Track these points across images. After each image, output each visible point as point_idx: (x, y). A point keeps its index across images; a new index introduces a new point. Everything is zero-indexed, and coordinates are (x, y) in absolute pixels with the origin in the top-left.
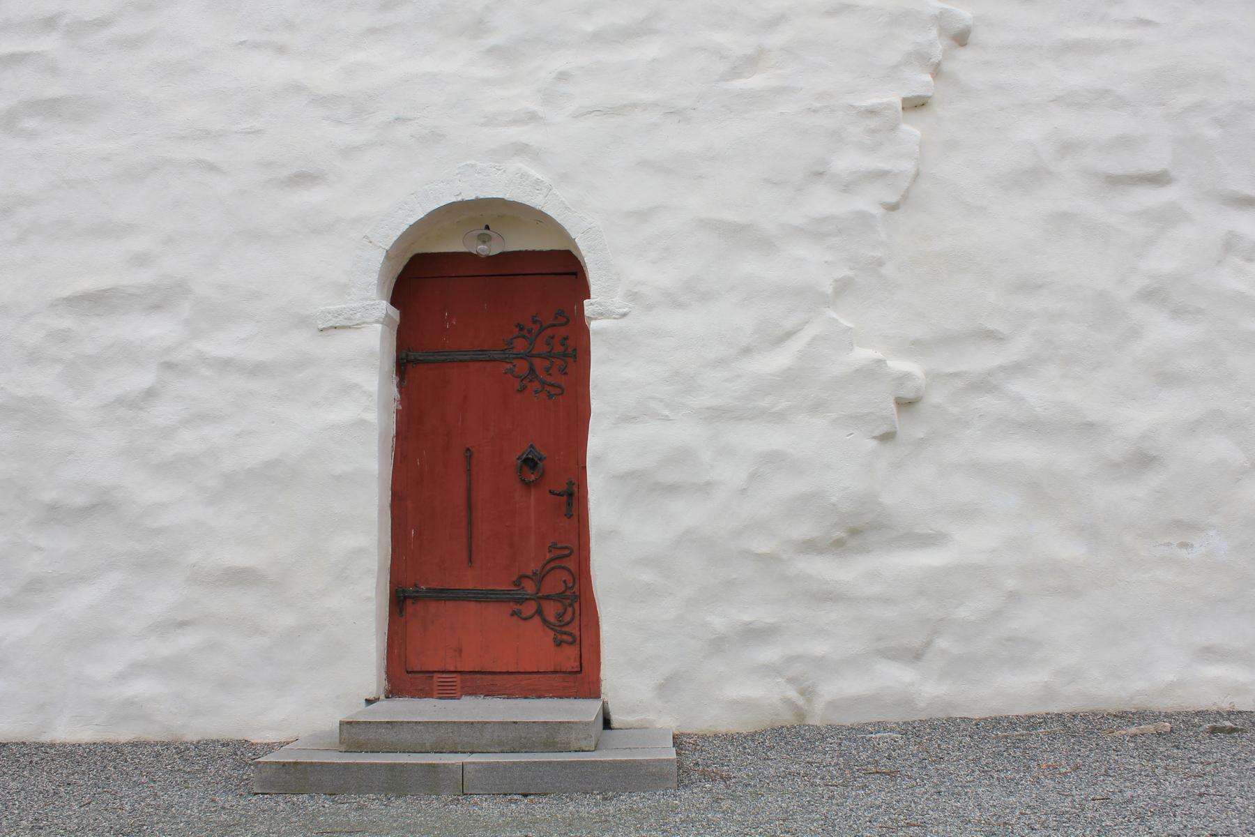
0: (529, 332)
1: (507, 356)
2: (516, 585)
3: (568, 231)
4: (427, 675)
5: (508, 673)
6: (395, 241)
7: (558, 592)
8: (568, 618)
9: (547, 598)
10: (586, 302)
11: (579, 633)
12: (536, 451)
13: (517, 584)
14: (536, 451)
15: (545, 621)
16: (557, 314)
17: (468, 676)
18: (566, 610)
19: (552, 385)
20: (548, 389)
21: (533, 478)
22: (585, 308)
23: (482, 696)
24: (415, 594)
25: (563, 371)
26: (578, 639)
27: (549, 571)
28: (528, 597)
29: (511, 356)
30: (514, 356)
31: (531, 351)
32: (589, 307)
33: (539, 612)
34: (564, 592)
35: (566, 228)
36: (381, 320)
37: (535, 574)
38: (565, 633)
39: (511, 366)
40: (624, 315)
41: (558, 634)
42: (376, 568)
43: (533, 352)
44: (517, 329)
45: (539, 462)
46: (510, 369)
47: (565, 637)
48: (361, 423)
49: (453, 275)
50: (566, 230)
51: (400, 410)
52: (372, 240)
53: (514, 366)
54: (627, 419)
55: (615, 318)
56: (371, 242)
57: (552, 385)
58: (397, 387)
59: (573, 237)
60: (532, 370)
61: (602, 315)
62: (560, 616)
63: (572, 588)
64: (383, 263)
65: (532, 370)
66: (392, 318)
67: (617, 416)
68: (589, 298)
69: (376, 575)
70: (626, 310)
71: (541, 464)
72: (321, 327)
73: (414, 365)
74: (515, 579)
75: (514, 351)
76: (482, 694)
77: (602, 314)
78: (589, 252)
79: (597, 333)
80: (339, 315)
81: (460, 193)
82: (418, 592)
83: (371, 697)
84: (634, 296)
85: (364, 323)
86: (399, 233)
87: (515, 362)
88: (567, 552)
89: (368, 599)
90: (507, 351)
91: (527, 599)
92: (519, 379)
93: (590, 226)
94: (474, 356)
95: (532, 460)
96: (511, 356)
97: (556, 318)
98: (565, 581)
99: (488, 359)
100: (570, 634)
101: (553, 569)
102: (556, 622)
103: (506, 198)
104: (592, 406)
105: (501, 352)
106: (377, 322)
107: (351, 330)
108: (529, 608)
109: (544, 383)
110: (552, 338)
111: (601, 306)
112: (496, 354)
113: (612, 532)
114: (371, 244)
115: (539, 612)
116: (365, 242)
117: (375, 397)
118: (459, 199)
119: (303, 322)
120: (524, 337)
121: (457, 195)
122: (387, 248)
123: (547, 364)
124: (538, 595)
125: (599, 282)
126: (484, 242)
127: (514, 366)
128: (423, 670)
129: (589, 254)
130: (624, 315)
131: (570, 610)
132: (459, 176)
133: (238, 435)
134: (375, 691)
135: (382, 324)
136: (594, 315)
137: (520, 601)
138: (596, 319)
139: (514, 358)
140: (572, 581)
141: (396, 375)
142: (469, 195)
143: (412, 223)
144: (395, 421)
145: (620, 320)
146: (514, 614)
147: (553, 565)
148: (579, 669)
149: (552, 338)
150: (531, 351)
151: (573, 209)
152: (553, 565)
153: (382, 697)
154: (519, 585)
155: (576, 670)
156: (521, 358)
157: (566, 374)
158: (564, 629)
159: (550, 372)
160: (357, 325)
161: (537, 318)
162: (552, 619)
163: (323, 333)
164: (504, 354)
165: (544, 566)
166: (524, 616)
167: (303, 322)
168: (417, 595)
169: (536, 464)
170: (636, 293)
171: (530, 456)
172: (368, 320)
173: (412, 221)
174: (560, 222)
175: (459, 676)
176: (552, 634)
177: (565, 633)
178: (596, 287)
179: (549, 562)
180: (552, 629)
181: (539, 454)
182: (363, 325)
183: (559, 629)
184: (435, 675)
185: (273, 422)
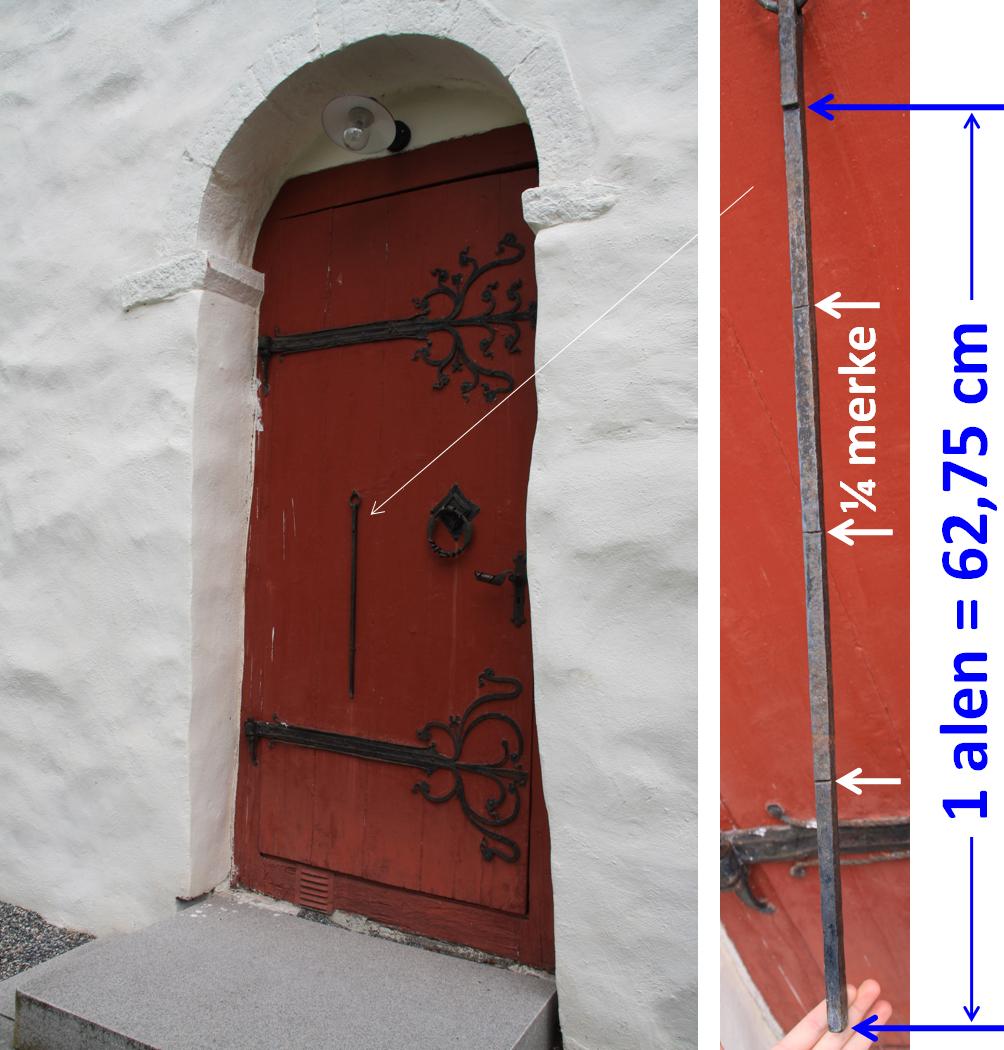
0: (456, 281)
1: (418, 328)
2: (421, 740)
3: (496, 64)
4: (289, 865)
5: (404, 889)
6: (224, 151)
7: (492, 764)
8: (508, 810)
9: (473, 770)
10: (527, 194)
11: (526, 845)
12: (463, 498)
13: (425, 736)
14: (463, 498)
15: (468, 812)
16: (501, 243)
17: (345, 881)
18: (504, 798)
19: (492, 375)
20: (484, 380)
21: (457, 547)
22: (525, 206)
23: (364, 919)
24: (271, 733)
25: (511, 348)
26: (524, 855)
27: (479, 721)
28: (442, 764)
29: (425, 328)
30: (430, 327)
31: (457, 316)
32: (533, 204)
33: (459, 794)
34: (501, 765)
35: (492, 60)
36: (201, 282)
37: (454, 724)
38: (501, 840)
39: (426, 346)
40: (604, 209)
41: (490, 840)
42: (190, 694)
43: (461, 317)
44: (437, 279)
45: (465, 519)
46: (424, 349)
47: (500, 847)
48: (169, 455)
49: (340, 204)
50: (492, 63)
51: (261, 433)
52: (192, 155)
53: (430, 345)
54: (612, 430)
55: (584, 219)
56: (191, 160)
57: (492, 375)
58: (259, 396)
59: (505, 75)
60: (458, 349)
61: (559, 216)
62: (494, 807)
63: (515, 759)
64: (209, 192)
65: (458, 349)
66: (239, 282)
67: (589, 425)
68: (536, 184)
69: (190, 705)
70: (609, 198)
71: (468, 524)
72: (125, 305)
73: (282, 358)
74: (421, 728)
75: (430, 319)
76: (365, 916)
77: (558, 215)
78: (536, 96)
79: (548, 254)
80: (147, 282)
81: (318, 46)
82: (276, 730)
83: (186, 895)
84: (625, 168)
85: (178, 290)
86: (229, 136)
87: (431, 338)
88: (511, 690)
89: (178, 743)
90: (418, 321)
91: (440, 767)
92: (437, 368)
93: (536, 44)
94: (367, 335)
95: (452, 514)
96: (425, 328)
97: (502, 251)
98: (505, 744)
99: (388, 337)
100: (512, 844)
101: (485, 717)
102: (487, 817)
103: (388, 33)
104: (541, 407)
105: (410, 323)
106: (196, 286)
107: (164, 305)
108: (444, 785)
109: (478, 372)
110: (494, 287)
111: (556, 196)
112: (399, 327)
113: (572, 670)
114: (191, 163)
115: (459, 794)
116: (185, 162)
117: (190, 411)
118: (317, 55)
119: (105, 300)
120: (447, 292)
121: (313, 50)
122: (213, 164)
123: (484, 335)
124: (457, 762)
125: (555, 152)
126: (359, 125)
127: (430, 345)
128: (281, 855)
129: (536, 100)
130: (604, 209)
131: (511, 797)
132: (316, 17)
133: (31, 477)
134: (188, 888)
135: (205, 288)
136: (541, 218)
137: (431, 769)
138: (545, 226)
139: (429, 332)
140: (517, 745)
141: (258, 377)
142: (331, 44)
143: (247, 115)
144: (254, 450)
145: (596, 221)
146: (418, 789)
147: (486, 710)
148: (523, 912)
149: (494, 287)
150: (457, 316)
151: (505, 19)
152: (486, 710)
153: (224, 888)
154: (428, 740)
155: (516, 911)
156: (443, 330)
157: (517, 352)
158: (501, 832)
159: (491, 350)
160: (170, 295)
161: (469, 256)
162: (481, 811)
163: (130, 314)
164: (413, 325)
165: (469, 713)
166: (433, 796)
167: (105, 300)
168: (276, 735)
169: (460, 523)
170: (630, 158)
171: (451, 508)
172: (182, 285)
173: (247, 112)
174: (480, 52)
175: (331, 880)
176: (479, 836)
177: (501, 840)
178: (550, 163)
179: (482, 702)
180: (481, 829)
181: (468, 503)
182: (177, 295)
183: (491, 830)
184: (300, 867)
185: (69, 457)
